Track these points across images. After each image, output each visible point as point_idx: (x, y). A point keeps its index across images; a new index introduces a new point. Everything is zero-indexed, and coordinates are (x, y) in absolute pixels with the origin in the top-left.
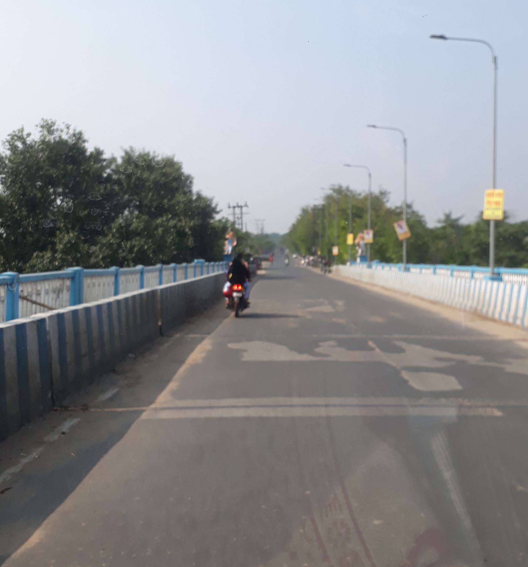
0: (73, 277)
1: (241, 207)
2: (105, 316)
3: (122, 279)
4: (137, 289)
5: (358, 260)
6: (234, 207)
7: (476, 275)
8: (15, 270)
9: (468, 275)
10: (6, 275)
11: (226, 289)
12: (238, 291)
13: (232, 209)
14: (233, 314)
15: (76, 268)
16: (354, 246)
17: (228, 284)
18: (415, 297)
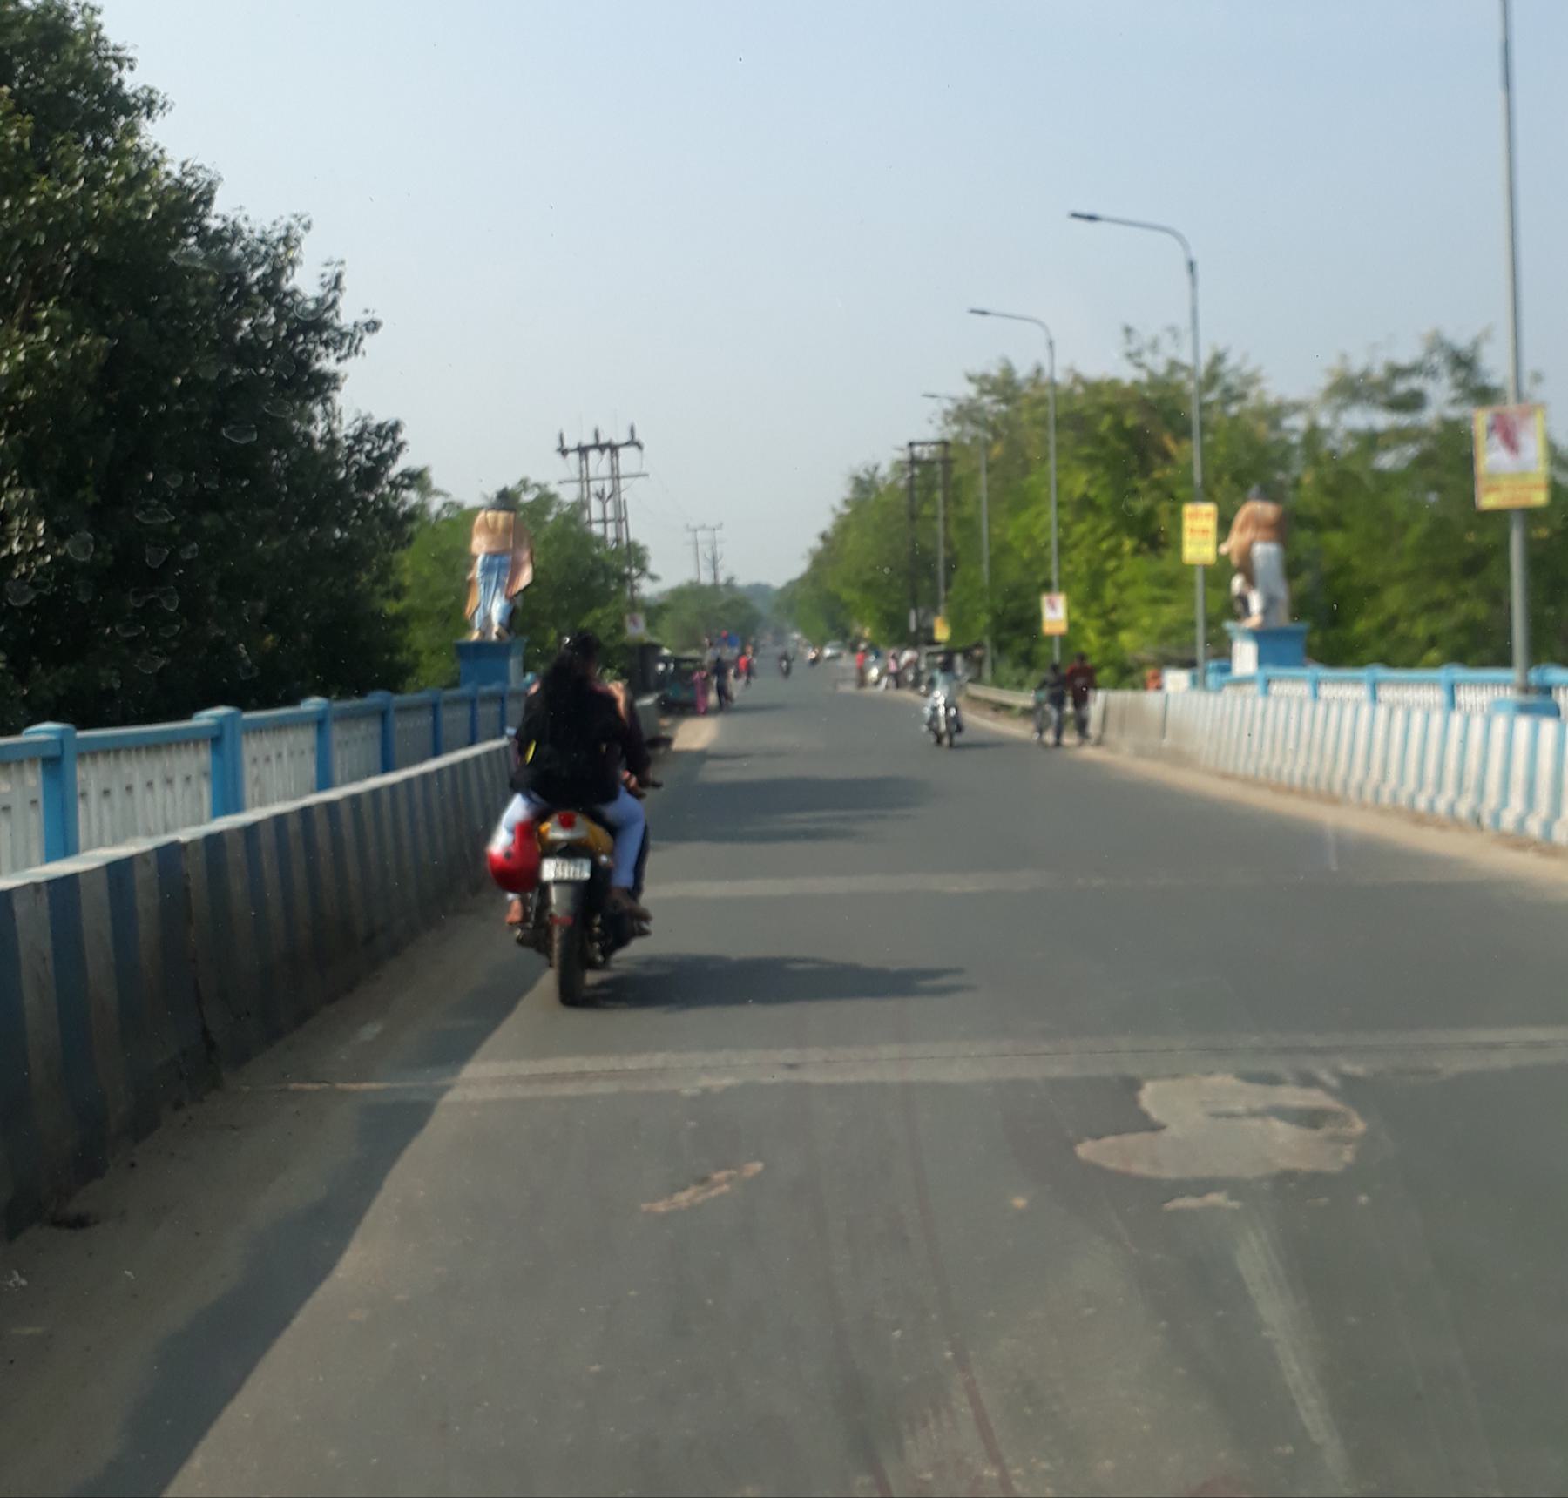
0: (216, 739)
1: (613, 448)
2: (268, 862)
3: (89, 776)
4: (312, 791)
5: (1245, 656)
6: (583, 450)
7: (1465, 696)
8: (253, 701)
9: (1303, 690)
10: (39, 732)
11: (501, 842)
12: (569, 851)
13: (573, 457)
14: (549, 980)
15: (221, 711)
16: (1218, 574)
17: (517, 809)
18: (1250, 781)
